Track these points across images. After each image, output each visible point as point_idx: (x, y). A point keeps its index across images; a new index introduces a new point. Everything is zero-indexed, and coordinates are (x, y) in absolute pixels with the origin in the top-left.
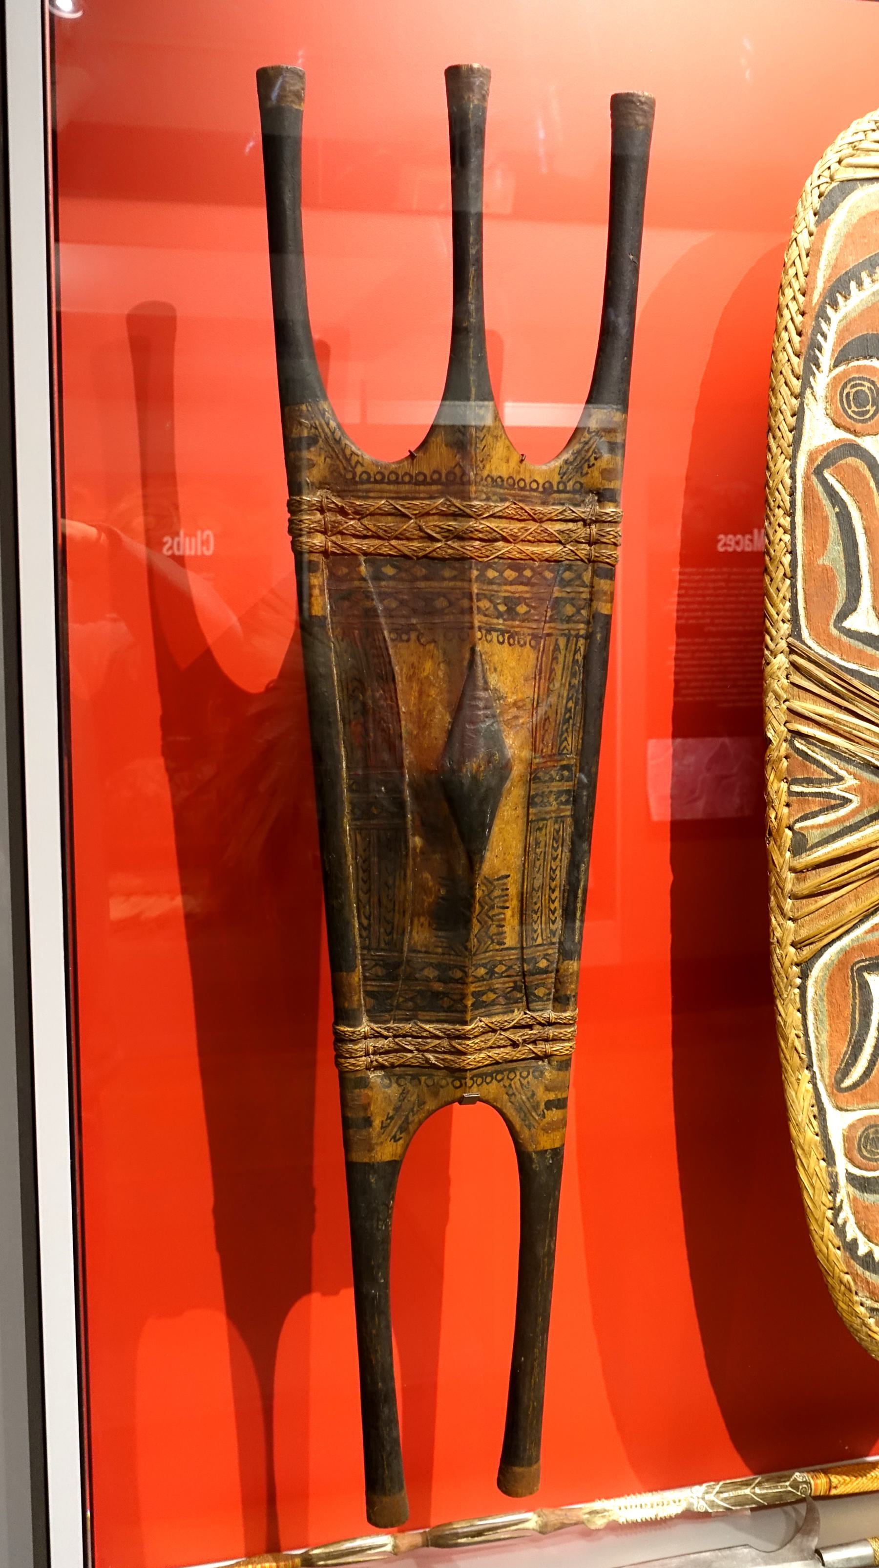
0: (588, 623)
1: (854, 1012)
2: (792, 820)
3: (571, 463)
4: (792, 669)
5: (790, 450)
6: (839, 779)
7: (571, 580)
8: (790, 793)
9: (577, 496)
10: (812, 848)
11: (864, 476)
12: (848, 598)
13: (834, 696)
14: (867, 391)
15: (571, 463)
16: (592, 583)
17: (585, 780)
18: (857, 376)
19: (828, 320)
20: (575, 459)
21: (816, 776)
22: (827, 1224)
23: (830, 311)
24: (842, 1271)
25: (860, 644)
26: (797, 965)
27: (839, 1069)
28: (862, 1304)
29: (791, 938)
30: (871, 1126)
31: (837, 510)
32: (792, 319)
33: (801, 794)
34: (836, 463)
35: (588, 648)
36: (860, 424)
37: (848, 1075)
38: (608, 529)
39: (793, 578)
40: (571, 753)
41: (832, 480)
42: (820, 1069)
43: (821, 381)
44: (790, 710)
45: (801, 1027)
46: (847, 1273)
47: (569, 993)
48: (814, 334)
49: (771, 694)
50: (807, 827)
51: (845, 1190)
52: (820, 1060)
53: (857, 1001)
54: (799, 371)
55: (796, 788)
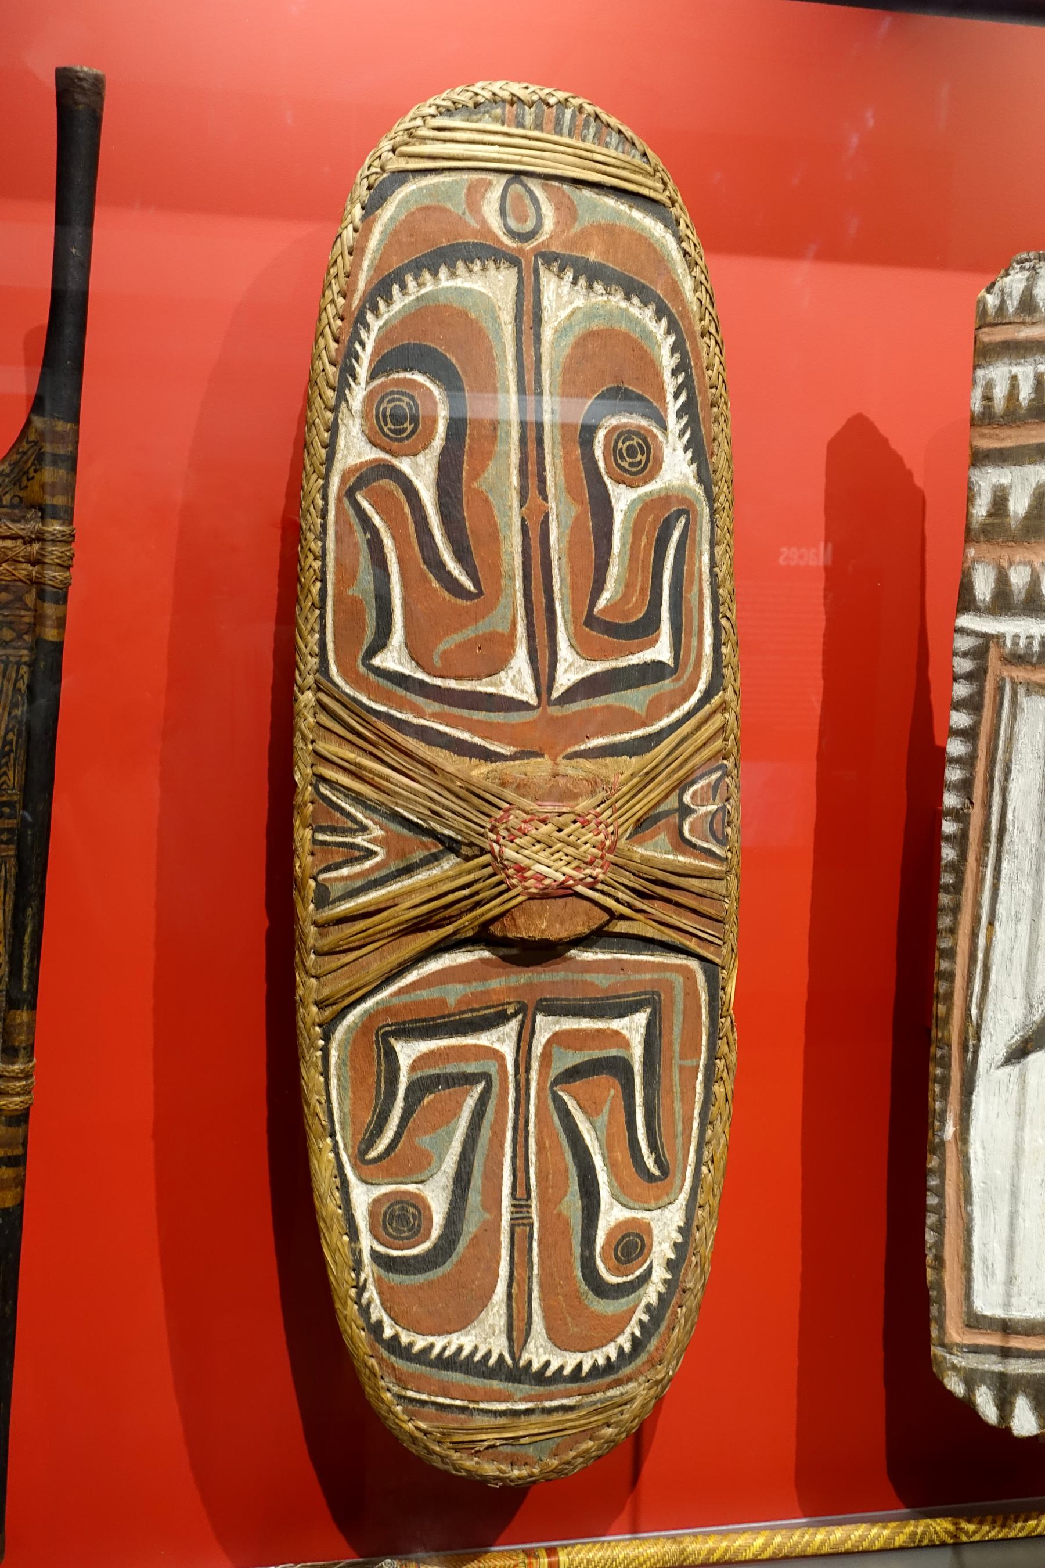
0: (31, 649)
1: (379, 1079)
2: (315, 871)
3: (8, 475)
4: (318, 708)
5: (323, 469)
6: (364, 829)
7: (7, 603)
8: (315, 841)
9: (16, 511)
10: (334, 902)
11: (398, 500)
12: (377, 633)
13: (679, 731)
14: (406, 407)
15: (8, 475)
16: (35, 605)
17: (29, 818)
18: (395, 389)
19: (367, 327)
20: (12, 471)
21: (340, 825)
22: (350, 1302)
23: (370, 317)
24: (365, 1354)
25: (389, 684)
26: (320, 1026)
27: (363, 1139)
28: (388, 1390)
29: (314, 996)
30: (397, 1203)
31: (369, 536)
32: (329, 324)
33: (324, 843)
34: (369, 484)
35: (32, 673)
36: (396, 443)
37: (372, 1146)
38: (50, 549)
39: (323, 607)
40: (14, 788)
41: (365, 504)
42: (343, 1138)
43: (358, 395)
44: (316, 753)
45: (323, 1093)
46: (372, 1356)
47: (17, 1044)
48: (351, 342)
49: (298, 734)
50: (330, 879)
51: (369, 1269)
52: (343, 1129)
53: (383, 1068)
54: (334, 381)
55: (321, 837)
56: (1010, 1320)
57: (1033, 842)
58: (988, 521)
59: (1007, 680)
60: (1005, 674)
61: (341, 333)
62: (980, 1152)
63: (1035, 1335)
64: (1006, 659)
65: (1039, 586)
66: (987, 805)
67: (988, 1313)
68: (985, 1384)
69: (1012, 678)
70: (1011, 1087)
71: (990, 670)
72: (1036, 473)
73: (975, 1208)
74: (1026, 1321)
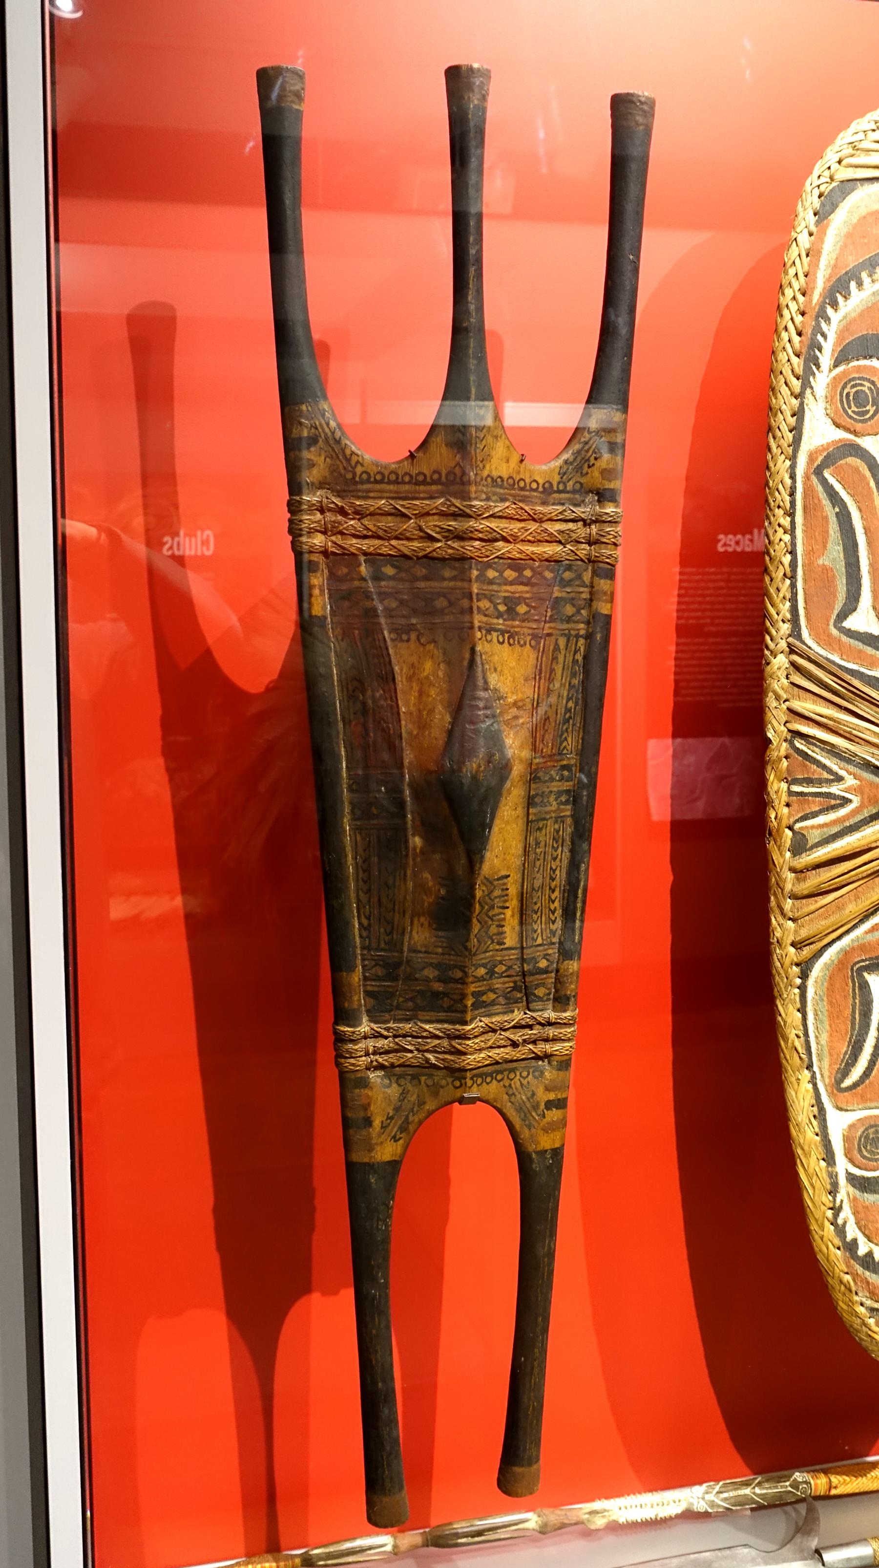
0: (588, 623)
1: (854, 1012)
2: (792, 820)
3: (571, 463)
4: (792, 669)
5: (790, 450)
6: (839, 779)
7: (571, 580)
8: (790, 793)
9: (577, 496)
10: (812, 848)
11: (864, 476)
12: (848, 598)
13: (834, 696)
14: (867, 391)
15: (571, 463)
16: (592, 583)
17: (585, 780)
18: (857, 376)
19: (828, 320)
20: (575, 459)
21: (816, 776)
22: (827, 1224)
23: (830, 311)
24: (842, 1271)
25: (860, 644)
26: (797, 965)
27: (839, 1069)
28: (862, 1304)
29: (791, 938)
30: (871, 1126)
31: (837, 510)
32: (792, 319)
33: (801, 794)
34: (836, 463)
35: (588, 648)
36: (860, 424)
37: (848, 1075)
38: (608, 529)
39: (793, 578)
40: (571, 753)
41: (832, 480)
42: (820, 1069)
43: (821, 381)
44: (790, 710)
45: (801, 1027)
46: (847, 1273)
47: (569, 993)
48: (814, 334)
49: (771, 694)
50: (807, 827)
51: (845, 1190)
52: (820, 1060)
53: (857, 1001)
54: (799, 371)
55: (796, 788)
61: (803, 326)
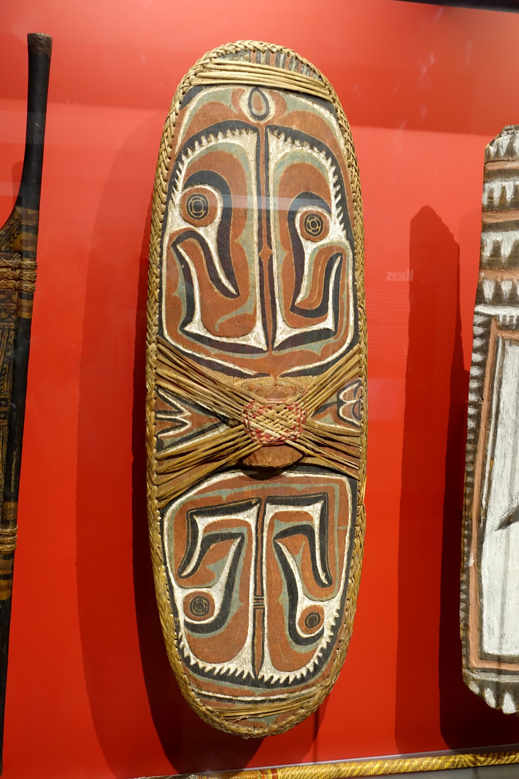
0: (15, 323)
1: (188, 536)
2: (157, 433)
3: (4, 236)
4: (158, 352)
5: (160, 233)
6: (181, 412)
7: (4, 300)
8: (156, 418)
9: (8, 254)
10: (166, 448)
11: (198, 248)
12: (187, 314)
13: (337, 363)
14: (201, 202)
15: (4, 236)
16: (18, 301)
17: (15, 407)
18: (196, 193)
19: (182, 162)
20: (6, 234)
21: (169, 410)
22: (174, 647)
23: (184, 157)
24: (181, 672)
25: (193, 340)
26: (159, 510)
27: (180, 566)
28: (193, 691)
29: (156, 495)
30: (197, 597)
31: (183, 266)
32: (163, 161)
33: (161, 419)
34: (183, 240)
35: (16, 335)
36: (197, 220)
37: (185, 569)
38: (25, 273)
39: (160, 302)
40: (7, 392)
41: (181, 251)
42: (170, 565)
43: (178, 196)
44: (157, 374)
45: (161, 543)
46: (185, 674)
47: (8, 519)
48: (175, 170)
49: (148, 365)
50: (164, 437)
51: (183, 630)
52: (170, 561)
53: (190, 531)
54: (166, 189)
55: (159, 416)
56: (502, 656)
57: (513, 418)
58: (491, 259)
59: (500, 338)
60: (499, 335)
61: (169, 166)
62: (487, 572)
63: (514, 663)
64: (499, 327)
65: (516, 291)
66: (490, 400)
67: (491, 652)
68: (489, 688)
69: (502, 337)
70: (502, 540)
71: (492, 333)
72: (515, 235)
73: (484, 600)
74: (510, 656)
